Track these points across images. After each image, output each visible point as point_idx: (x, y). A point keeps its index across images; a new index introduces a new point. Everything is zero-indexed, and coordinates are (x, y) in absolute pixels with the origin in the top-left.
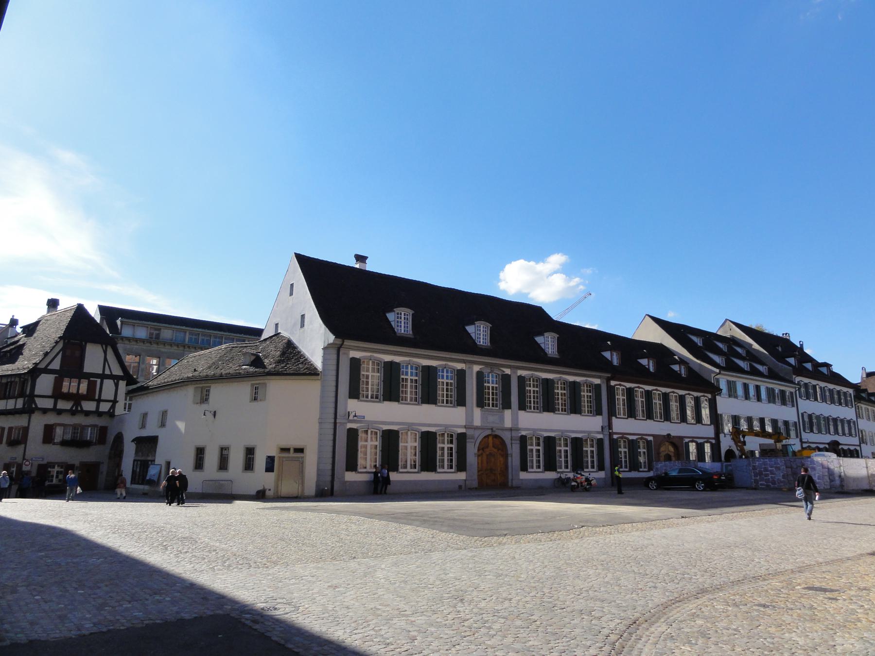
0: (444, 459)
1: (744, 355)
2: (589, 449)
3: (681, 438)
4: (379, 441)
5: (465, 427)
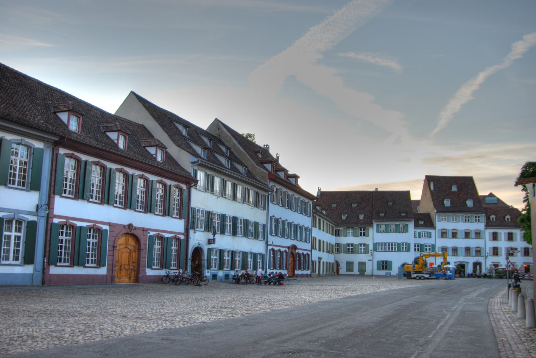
0: (9, 249)
4: (24, 232)
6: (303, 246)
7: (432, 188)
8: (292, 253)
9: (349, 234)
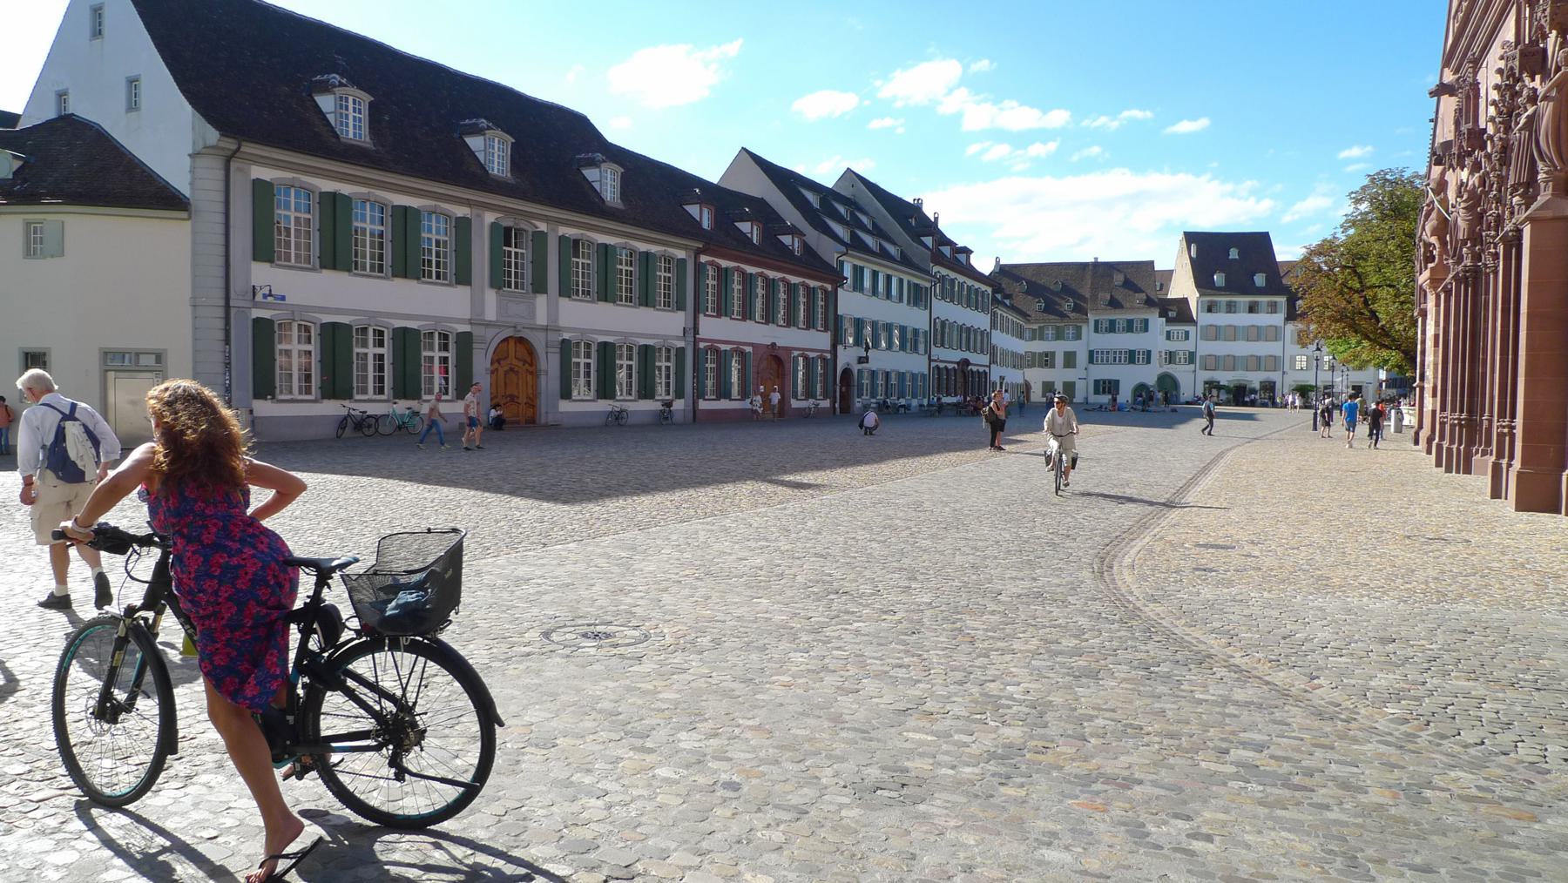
1: (870, 227)
2: (663, 364)
3: (789, 350)
5: (470, 322)
6: (978, 360)
7: (1193, 254)
8: (963, 372)
9: (1050, 332)
